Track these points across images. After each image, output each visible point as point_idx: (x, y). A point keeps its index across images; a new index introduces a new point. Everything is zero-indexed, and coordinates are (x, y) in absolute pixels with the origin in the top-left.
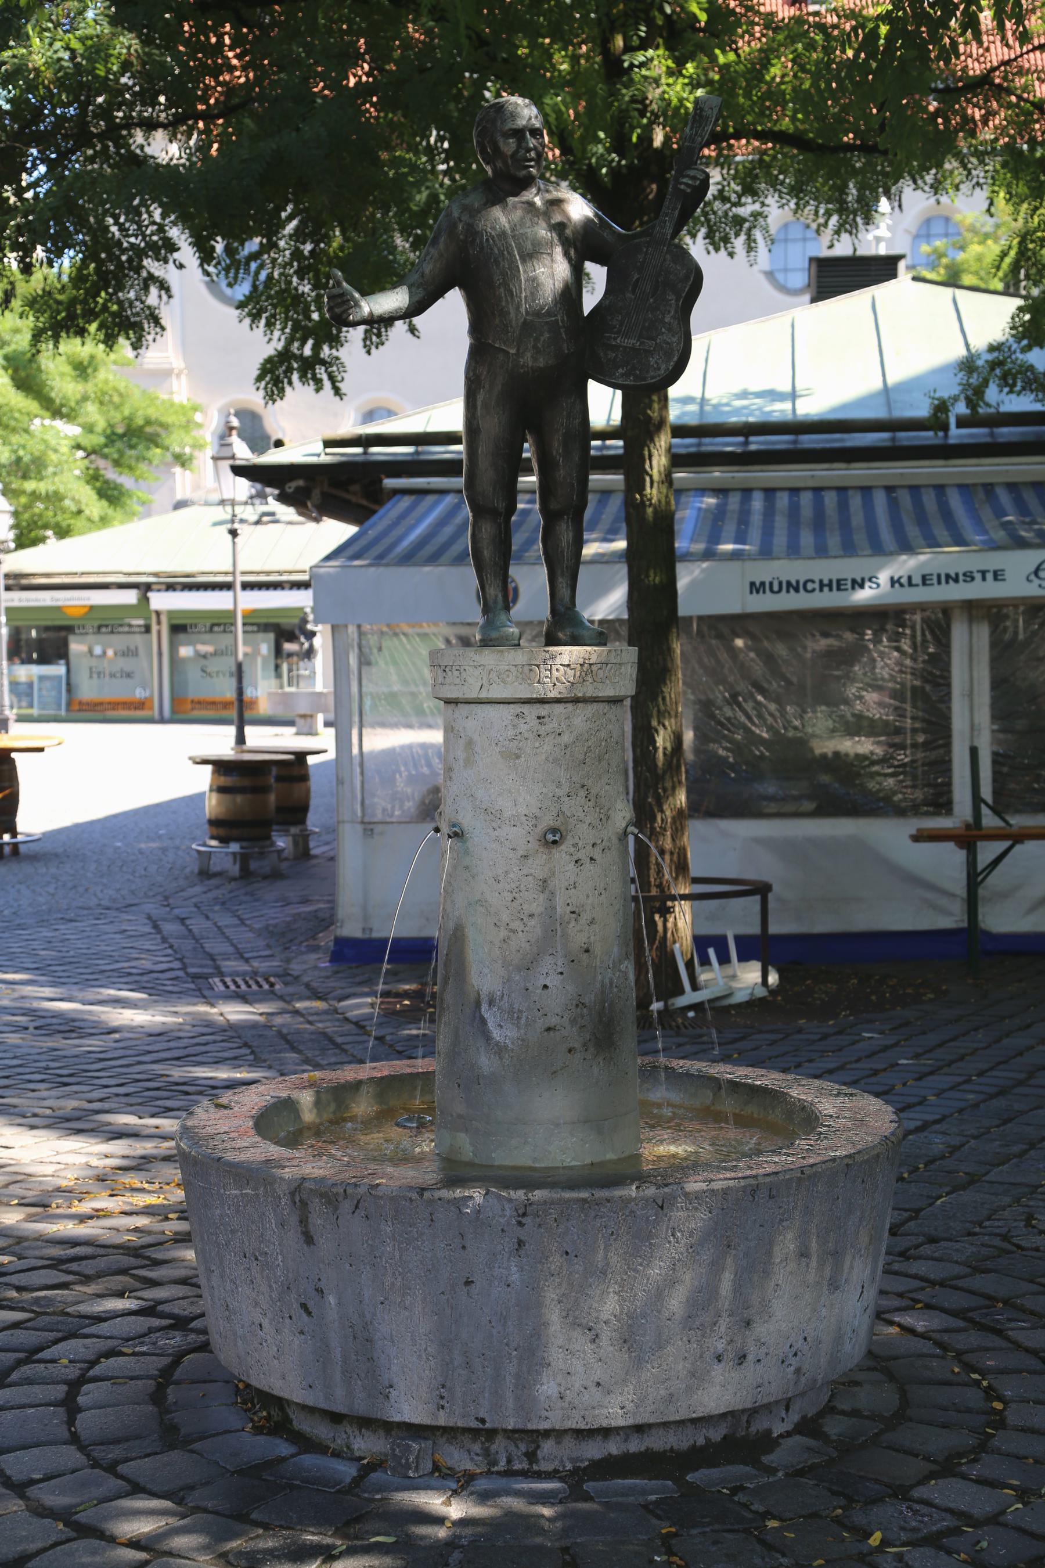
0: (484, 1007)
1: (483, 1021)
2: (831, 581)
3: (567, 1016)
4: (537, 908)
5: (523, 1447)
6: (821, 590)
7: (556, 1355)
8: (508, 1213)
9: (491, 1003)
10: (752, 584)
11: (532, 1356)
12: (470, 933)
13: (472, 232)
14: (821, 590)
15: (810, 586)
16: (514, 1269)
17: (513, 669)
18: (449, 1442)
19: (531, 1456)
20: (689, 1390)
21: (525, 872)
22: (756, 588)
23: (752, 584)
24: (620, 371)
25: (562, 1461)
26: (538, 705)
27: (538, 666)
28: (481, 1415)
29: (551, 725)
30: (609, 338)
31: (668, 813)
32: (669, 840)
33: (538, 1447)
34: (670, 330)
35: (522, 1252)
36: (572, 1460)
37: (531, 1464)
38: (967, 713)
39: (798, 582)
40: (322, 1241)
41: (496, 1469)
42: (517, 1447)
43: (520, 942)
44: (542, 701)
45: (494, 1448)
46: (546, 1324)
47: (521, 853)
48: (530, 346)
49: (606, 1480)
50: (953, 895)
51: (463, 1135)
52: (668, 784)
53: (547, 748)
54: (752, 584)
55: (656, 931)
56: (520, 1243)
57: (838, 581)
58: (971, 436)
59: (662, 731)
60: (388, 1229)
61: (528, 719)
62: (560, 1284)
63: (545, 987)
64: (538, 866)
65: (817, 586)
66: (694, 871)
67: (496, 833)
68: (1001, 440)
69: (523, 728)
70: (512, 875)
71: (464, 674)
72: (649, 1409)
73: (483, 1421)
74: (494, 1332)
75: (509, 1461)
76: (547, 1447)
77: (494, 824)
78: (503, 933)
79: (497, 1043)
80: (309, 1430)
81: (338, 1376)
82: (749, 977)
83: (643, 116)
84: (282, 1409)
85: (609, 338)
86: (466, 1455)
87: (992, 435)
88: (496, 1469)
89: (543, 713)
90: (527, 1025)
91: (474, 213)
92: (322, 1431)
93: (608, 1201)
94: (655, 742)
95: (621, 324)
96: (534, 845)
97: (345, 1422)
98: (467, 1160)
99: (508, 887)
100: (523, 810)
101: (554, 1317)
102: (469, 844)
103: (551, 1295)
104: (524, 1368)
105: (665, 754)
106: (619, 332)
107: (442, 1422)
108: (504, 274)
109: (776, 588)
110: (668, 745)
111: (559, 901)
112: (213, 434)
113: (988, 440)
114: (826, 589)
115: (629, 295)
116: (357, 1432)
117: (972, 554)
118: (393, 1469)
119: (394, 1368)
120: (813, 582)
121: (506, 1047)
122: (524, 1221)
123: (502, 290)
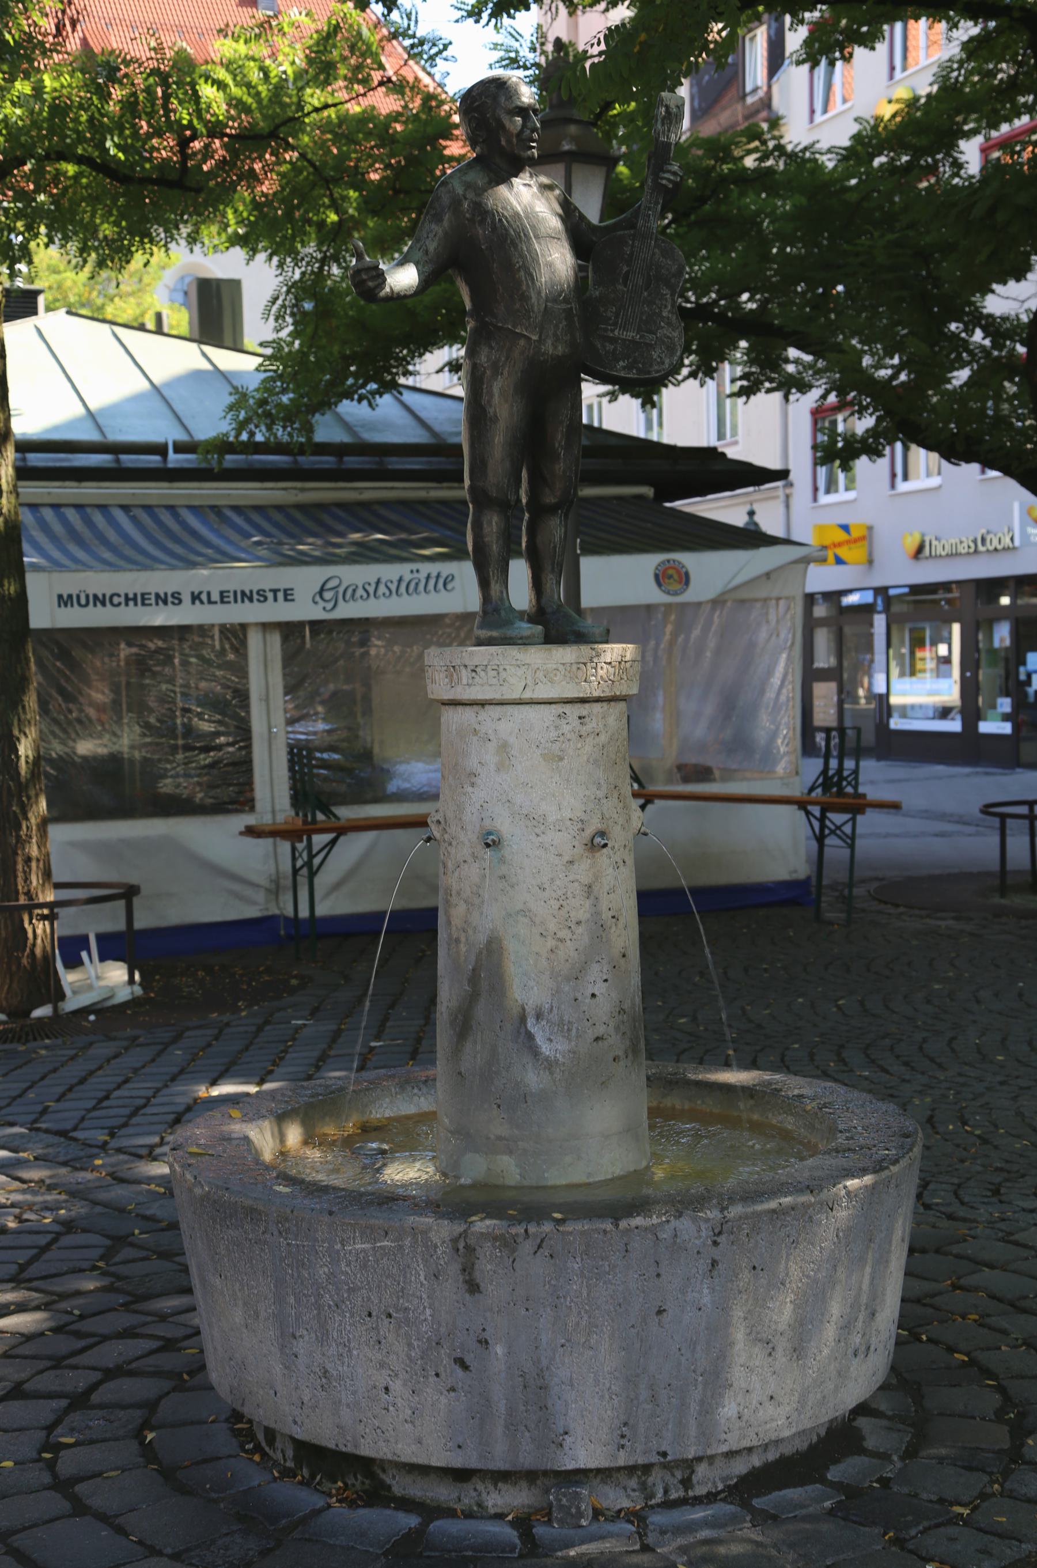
0: (530, 1022)
1: (530, 1037)
2: (135, 595)
3: (612, 1024)
4: (583, 914)
5: (679, 1474)
6: (127, 605)
7: (738, 1376)
8: (704, 1234)
9: (539, 1016)
10: (60, 597)
11: (716, 1380)
12: (511, 946)
13: (482, 213)
14: (127, 605)
15: (116, 600)
16: (706, 1291)
17: (561, 668)
18: (604, 1482)
19: (686, 1483)
20: (837, 1389)
21: (571, 878)
22: (64, 601)
23: (60, 597)
24: (621, 363)
25: (714, 1483)
26: (579, 705)
27: (585, 664)
28: (663, 1449)
29: (591, 725)
30: (606, 330)
31: (33, 821)
32: (35, 848)
33: (693, 1472)
34: (669, 324)
35: (715, 1273)
36: (723, 1480)
37: (686, 1491)
38: (265, 718)
39: (104, 596)
40: (490, 1288)
41: (653, 1502)
42: (673, 1475)
43: (569, 951)
44: (583, 701)
45: (650, 1480)
46: (732, 1344)
47: (567, 858)
48: (551, 333)
49: (765, 1494)
50: (258, 886)
51: (506, 1158)
52: (32, 793)
53: (588, 748)
54: (60, 597)
55: (27, 938)
56: (714, 1263)
57: (143, 595)
58: (188, 461)
59: (23, 740)
60: (576, 1266)
61: (570, 720)
62: (747, 1301)
63: (593, 995)
64: (583, 872)
65: (122, 600)
66: (58, 877)
67: (540, 839)
68: (124, 465)
69: (566, 729)
70: (558, 882)
71: (503, 675)
72: (808, 1415)
73: (664, 1454)
74: (683, 1359)
75: (666, 1492)
76: (702, 1470)
77: (537, 830)
78: (551, 943)
79: (547, 1059)
80: (419, 1494)
81: (499, 1430)
82: (115, 977)
83: (40, 129)
84: (371, 1475)
85: (606, 330)
86: (622, 1492)
87: (118, 461)
88: (653, 1502)
89: (584, 713)
90: (578, 1036)
91: (481, 191)
92: (443, 1493)
93: (793, 1209)
94: (17, 750)
95: (617, 316)
96: (580, 849)
97: (475, 1480)
98: (512, 1183)
99: (554, 895)
100: (567, 814)
101: (739, 1335)
102: (506, 852)
103: (738, 1313)
104: (709, 1393)
105: (27, 762)
106: (615, 324)
107: (621, 1462)
109: (83, 601)
110: (30, 753)
111: (604, 905)
112: (495, 419)
113: (113, 465)
114: (131, 603)
115: (620, 287)
116: (491, 1488)
117: (258, 571)
118: (561, 1522)
119: (571, 1414)
120: (119, 596)
121: (557, 1061)
122: (719, 1240)
123: (522, 273)
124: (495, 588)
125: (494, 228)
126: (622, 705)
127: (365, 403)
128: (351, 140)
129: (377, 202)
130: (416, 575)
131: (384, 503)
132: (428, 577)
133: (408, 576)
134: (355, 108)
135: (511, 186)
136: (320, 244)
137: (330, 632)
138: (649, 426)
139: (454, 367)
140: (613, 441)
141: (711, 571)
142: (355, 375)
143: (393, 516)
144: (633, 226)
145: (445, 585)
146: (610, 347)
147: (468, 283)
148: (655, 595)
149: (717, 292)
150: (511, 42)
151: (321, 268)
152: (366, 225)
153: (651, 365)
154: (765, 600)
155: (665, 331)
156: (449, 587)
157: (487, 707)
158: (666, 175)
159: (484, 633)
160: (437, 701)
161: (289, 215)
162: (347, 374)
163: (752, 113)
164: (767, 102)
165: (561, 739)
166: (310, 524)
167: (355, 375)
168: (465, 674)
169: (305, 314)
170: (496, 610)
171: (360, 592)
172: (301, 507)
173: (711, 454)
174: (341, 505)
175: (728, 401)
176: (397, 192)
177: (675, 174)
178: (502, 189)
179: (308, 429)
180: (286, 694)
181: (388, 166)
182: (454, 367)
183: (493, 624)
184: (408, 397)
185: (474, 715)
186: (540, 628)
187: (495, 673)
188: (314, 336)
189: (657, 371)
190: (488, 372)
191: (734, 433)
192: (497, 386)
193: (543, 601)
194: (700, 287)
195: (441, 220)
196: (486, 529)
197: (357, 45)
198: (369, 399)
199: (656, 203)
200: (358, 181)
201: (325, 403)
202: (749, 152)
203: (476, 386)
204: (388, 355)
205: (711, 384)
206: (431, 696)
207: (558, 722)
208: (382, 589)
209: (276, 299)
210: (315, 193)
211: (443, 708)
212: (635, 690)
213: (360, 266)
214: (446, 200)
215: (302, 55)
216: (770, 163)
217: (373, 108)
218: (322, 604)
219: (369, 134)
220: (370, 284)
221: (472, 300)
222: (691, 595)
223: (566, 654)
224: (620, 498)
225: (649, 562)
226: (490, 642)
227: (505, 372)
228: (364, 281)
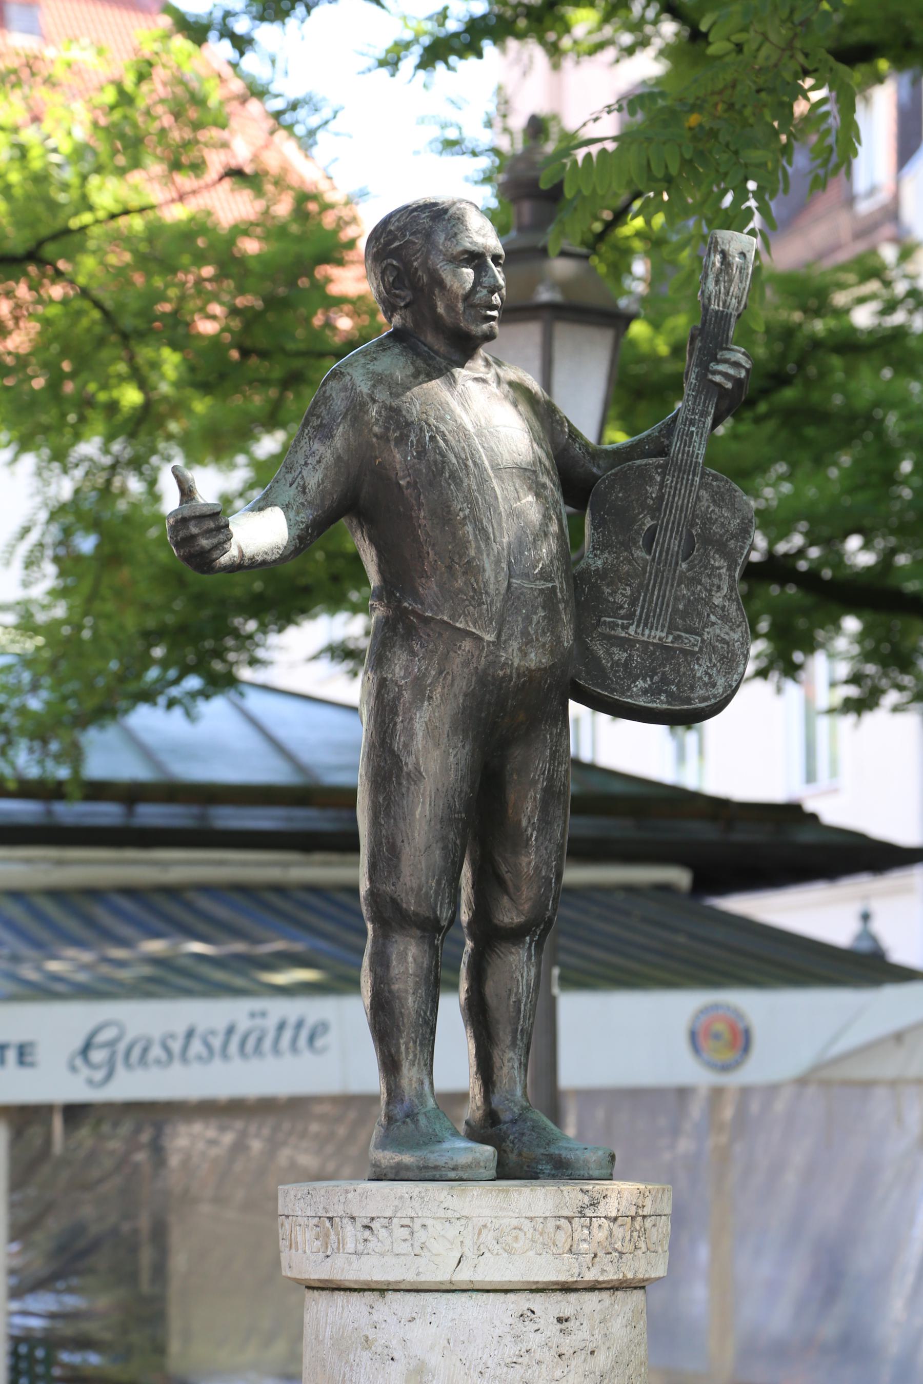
24: (640, 683)
26: (558, 1296)
27: (569, 1219)
29: (580, 1335)
30: (613, 626)
34: (725, 618)
44: (566, 1288)
48: (517, 630)
61: (541, 1324)
71: (421, 1235)
85: (613, 626)
89: (567, 1312)
91: (399, 389)
95: (633, 602)
106: (630, 616)
108: (470, 501)
112: (417, 776)
115: (640, 553)
123: (469, 528)
124: (409, 1074)
125: (422, 453)
126: (638, 1295)
127: (178, 712)
128: (169, 267)
129: (211, 372)
130: (258, 1022)
131: (207, 889)
132: (281, 1026)
133: (244, 1024)
134: (178, 213)
135: (452, 382)
136: (110, 438)
137: (99, 1123)
138: (681, 756)
139: (341, 652)
140: (617, 787)
141: (791, 1026)
142: (165, 664)
143: (221, 911)
144: (663, 451)
145: (312, 1039)
146: (620, 655)
147: (373, 541)
148: (689, 1071)
149: (806, 534)
150: (450, 114)
151: (109, 482)
152: (190, 411)
153: (692, 688)
154: (894, 1084)
155: (717, 630)
156: (319, 1043)
157: (390, 1295)
158: (722, 367)
159: (388, 1157)
160: (298, 1281)
161: (54, 386)
162: (146, 662)
163: (866, 230)
164: (892, 213)
165: (525, 1360)
166: (72, 925)
167: (165, 664)
168: (351, 1234)
169: (78, 558)
170: (411, 1115)
171: (156, 1051)
172: (57, 894)
173: (791, 814)
174: (130, 892)
175: (823, 724)
176: (245, 353)
177: (737, 365)
178: (436, 386)
179: (74, 755)
180: (12, 1239)
181: (234, 311)
182: (341, 652)
183: (399, 1135)
184: (255, 702)
185: (365, 1310)
186: (488, 1150)
187: (405, 1232)
188: (93, 596)
189: (704, 699)
190: (407, 695)
191: (834, 771)
192: (421, 719)
193: (496, 1099)
194: (776, 523)
195: (330, 436)
196: (396, 969)
197: (189, 105)
198: (185, 705)
199: (704, 414)
200: (177, 331)
201: (105, 711)
202: (861, 300)
203: (385, 711)
204: (222, 629)
205: (792, 689)
206: (286, 1272)
207: (519, 1326)
208: (197, 1047)
209: (26, 531)
210: (105, 354)
211: (309, 1294)
212: (660, 1271)
213: (187, 513)
214: (339, 403)
215: (87, 117)
216: (898, 318)
217: (209, 214)
218: (85, 1072)
219: (200, 258)
220: (205, 543)
221: (381, 571)
222: (756, 1071)
223: (536, 1199)
224: (630, 889)
225: (679, 1007)
226: (397, 1174)
227: (437, 696)
228: (193, 537)
